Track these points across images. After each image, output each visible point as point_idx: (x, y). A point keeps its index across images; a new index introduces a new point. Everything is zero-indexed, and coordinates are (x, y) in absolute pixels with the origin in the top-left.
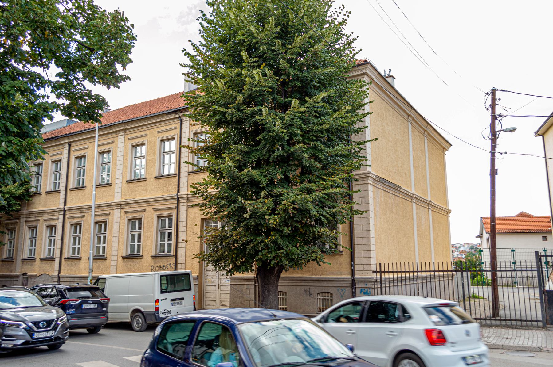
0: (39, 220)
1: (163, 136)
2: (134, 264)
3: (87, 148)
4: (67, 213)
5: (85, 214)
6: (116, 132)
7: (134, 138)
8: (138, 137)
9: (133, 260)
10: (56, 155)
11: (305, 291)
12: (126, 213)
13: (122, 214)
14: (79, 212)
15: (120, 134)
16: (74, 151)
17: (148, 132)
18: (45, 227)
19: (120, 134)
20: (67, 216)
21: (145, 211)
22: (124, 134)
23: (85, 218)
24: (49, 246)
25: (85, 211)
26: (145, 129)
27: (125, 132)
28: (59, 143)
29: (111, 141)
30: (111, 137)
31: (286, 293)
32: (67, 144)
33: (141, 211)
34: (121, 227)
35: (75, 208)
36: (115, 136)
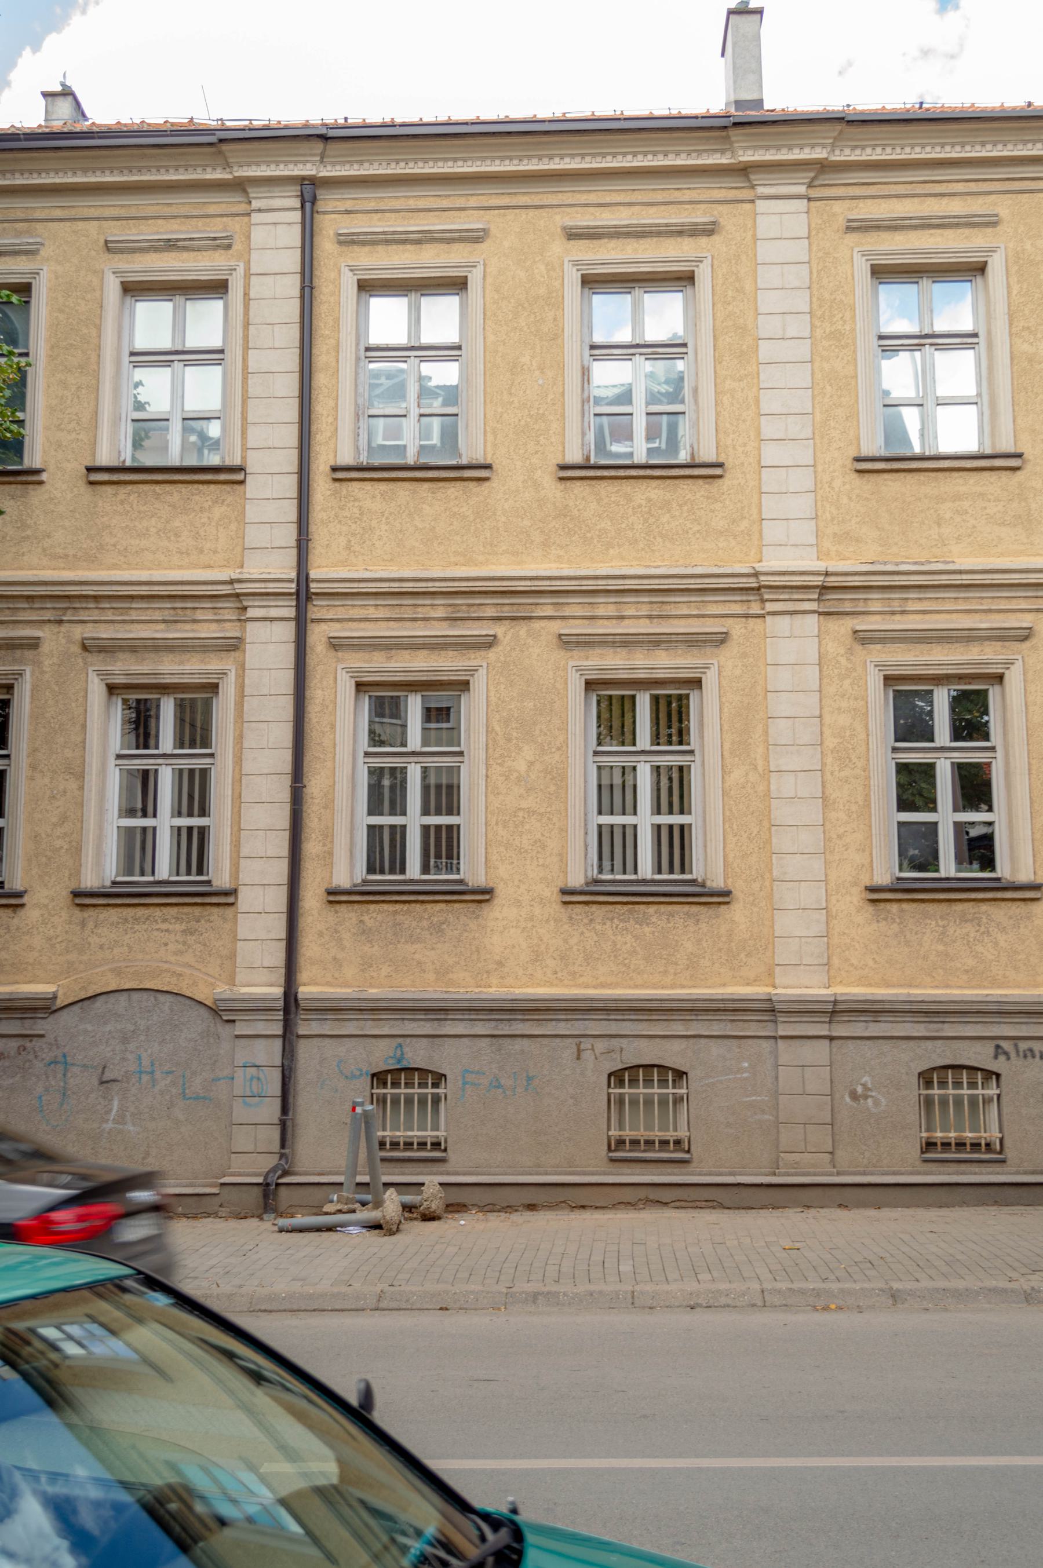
0: (34, 644)
1: (884, 247)
2: (969, 928)
3: (709, 230)
4: (316, 610)
5: (499, 630)
6: (744, 171)
7: (895, 226)
8: (925, 224)
9: (959, 907)
10: (171, 245)
11: (233, 1079)
12: (863, 638)
13: (832, 648)
14: (440, 613)
15: (761, 190)
16: (348, 241)
17: (1003, 207)
18: (97, 689)
19: (761, 190)
20: (318, 636)
21: (1025, 639)
22: (802, 189)
23: (492, 654)
24: (371, 812)
25: (490, 612)
26: (973, 187)
27: (810, 186)
28: (218, 175)
29: (699, 216)
30: (688, 195)
31: (998, 1076)
32: (295, 190)
33: (693, 641)
34: (828, 719)
35: (408, 586)
36: (732, 194)
